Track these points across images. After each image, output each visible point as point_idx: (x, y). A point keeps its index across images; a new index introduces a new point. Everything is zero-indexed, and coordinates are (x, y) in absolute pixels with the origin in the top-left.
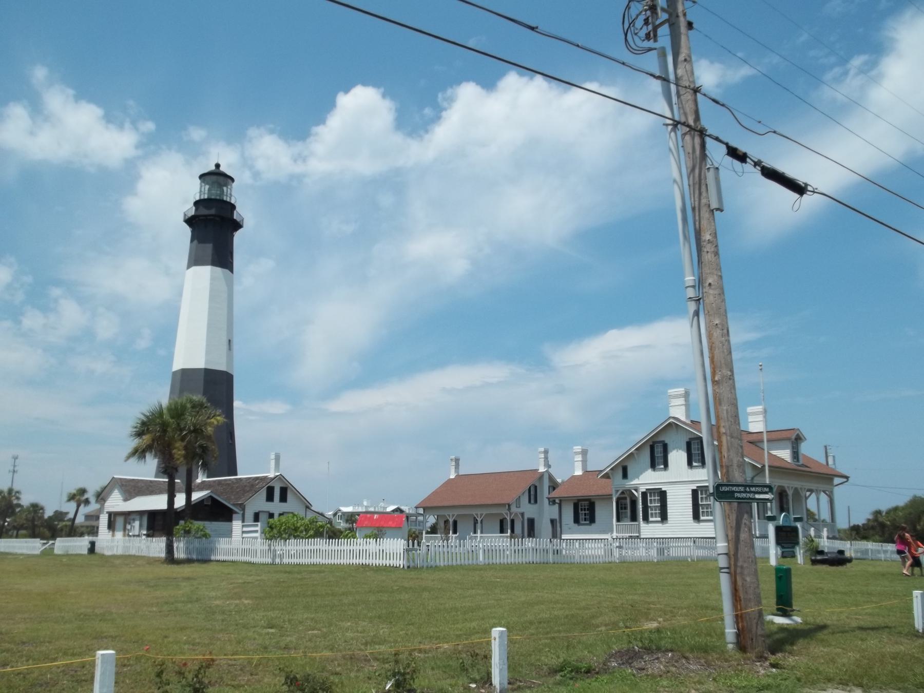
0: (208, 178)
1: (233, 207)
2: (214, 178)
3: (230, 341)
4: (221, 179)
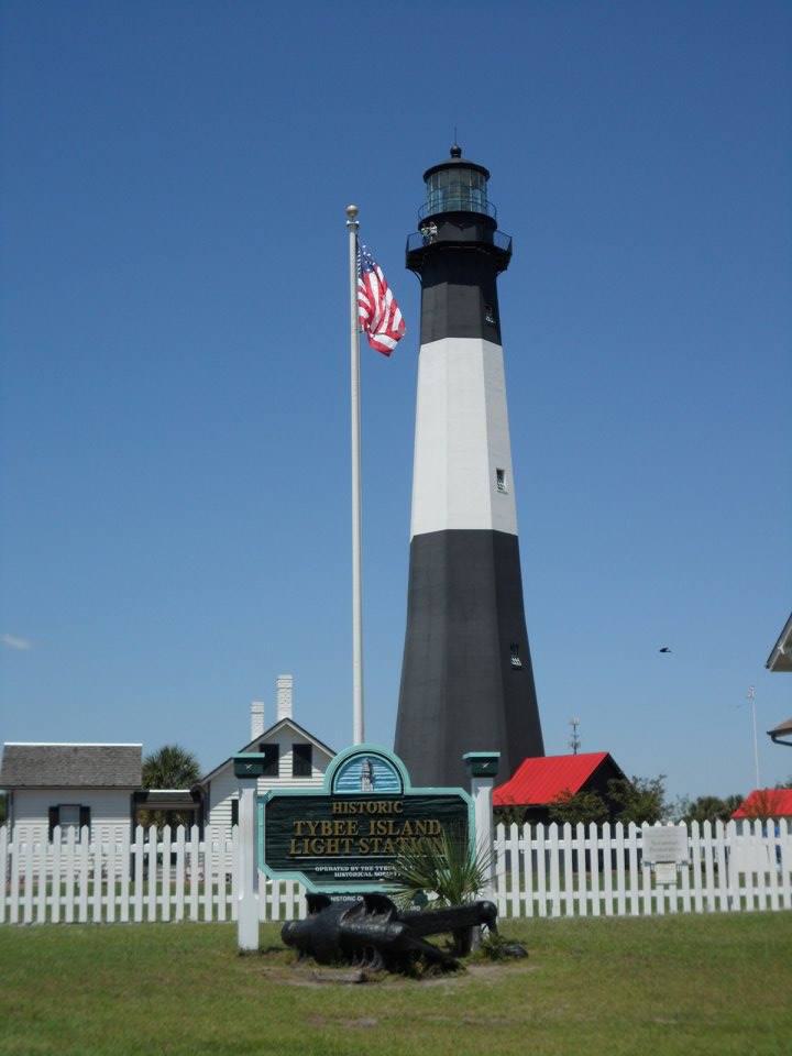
0: (442, 178)
2: (453, 174)
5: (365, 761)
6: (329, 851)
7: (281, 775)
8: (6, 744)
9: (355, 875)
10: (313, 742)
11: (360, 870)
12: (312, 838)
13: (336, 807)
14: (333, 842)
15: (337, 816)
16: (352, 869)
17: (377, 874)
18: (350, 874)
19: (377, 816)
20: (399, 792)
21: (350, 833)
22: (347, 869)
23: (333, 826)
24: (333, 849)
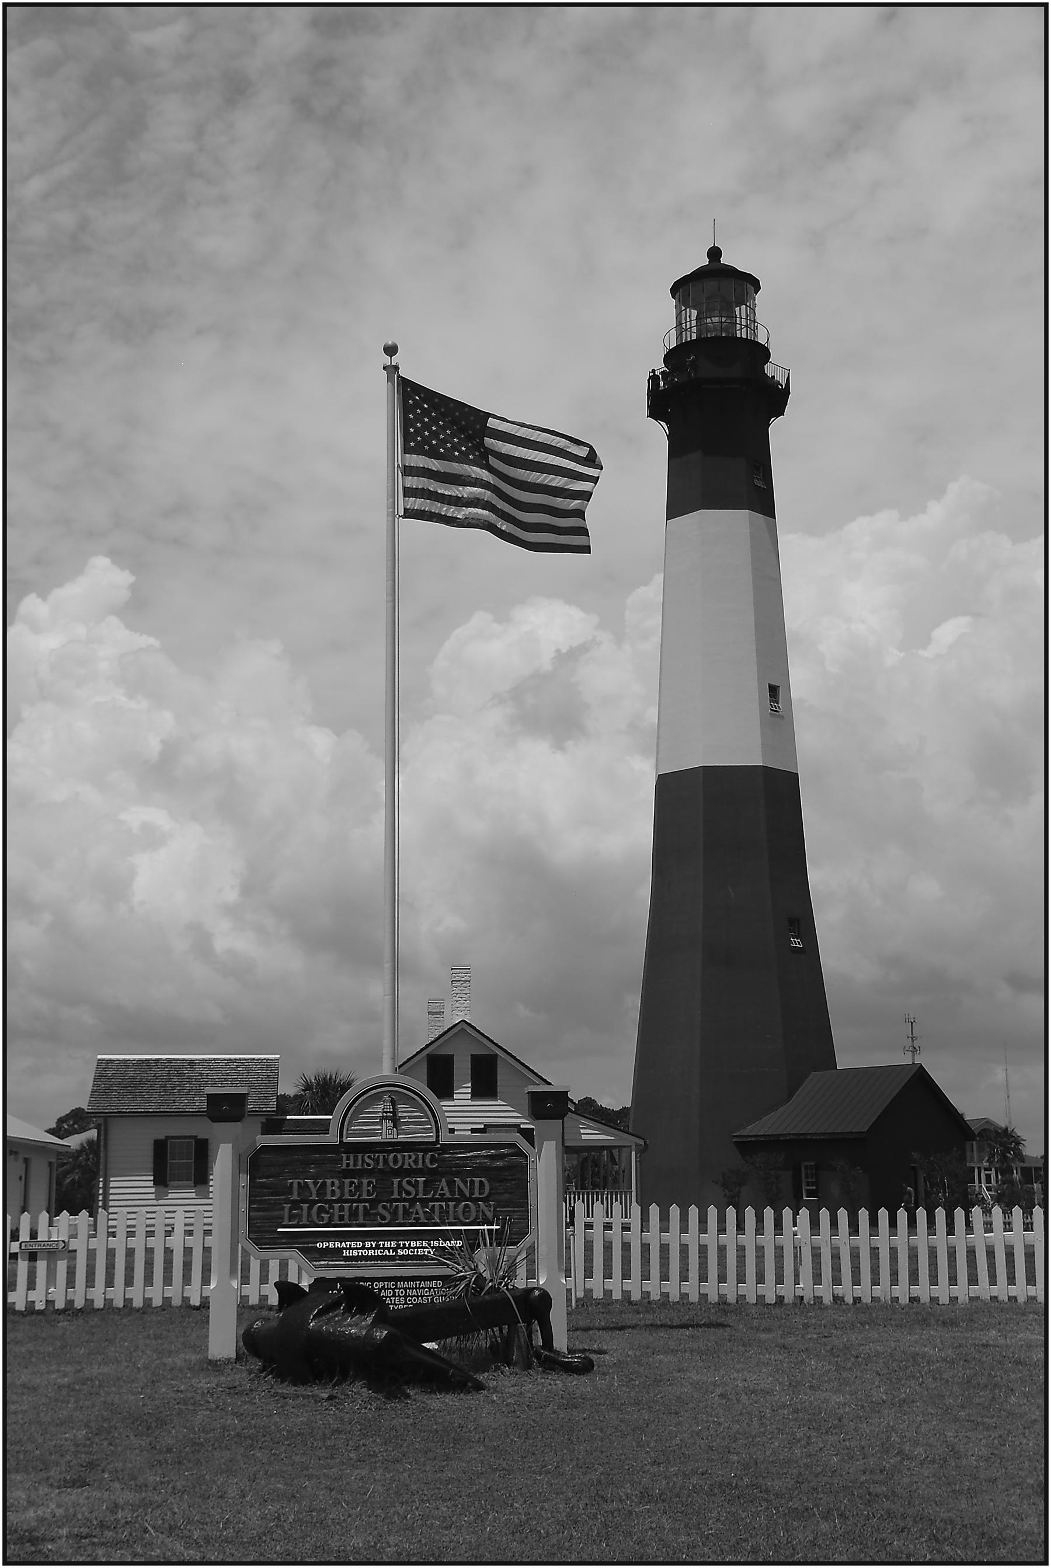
1: (763, 353)
2: (711, 284)
3: (774, 691)
6: (304, 1221)
8: (99, 1057)
9: (371, 1252)
10: (426, 1052)
12: (313, 1203)
13: (347, 1161)
14: (342, 1209)
15: (348, 1173)
16: (368, 1244)
17: (400, 1252)
19: (401, 1173)
21: (365, 1196)
22: (360, 1244)
23: (341, 1187)
24: (341, 1218)
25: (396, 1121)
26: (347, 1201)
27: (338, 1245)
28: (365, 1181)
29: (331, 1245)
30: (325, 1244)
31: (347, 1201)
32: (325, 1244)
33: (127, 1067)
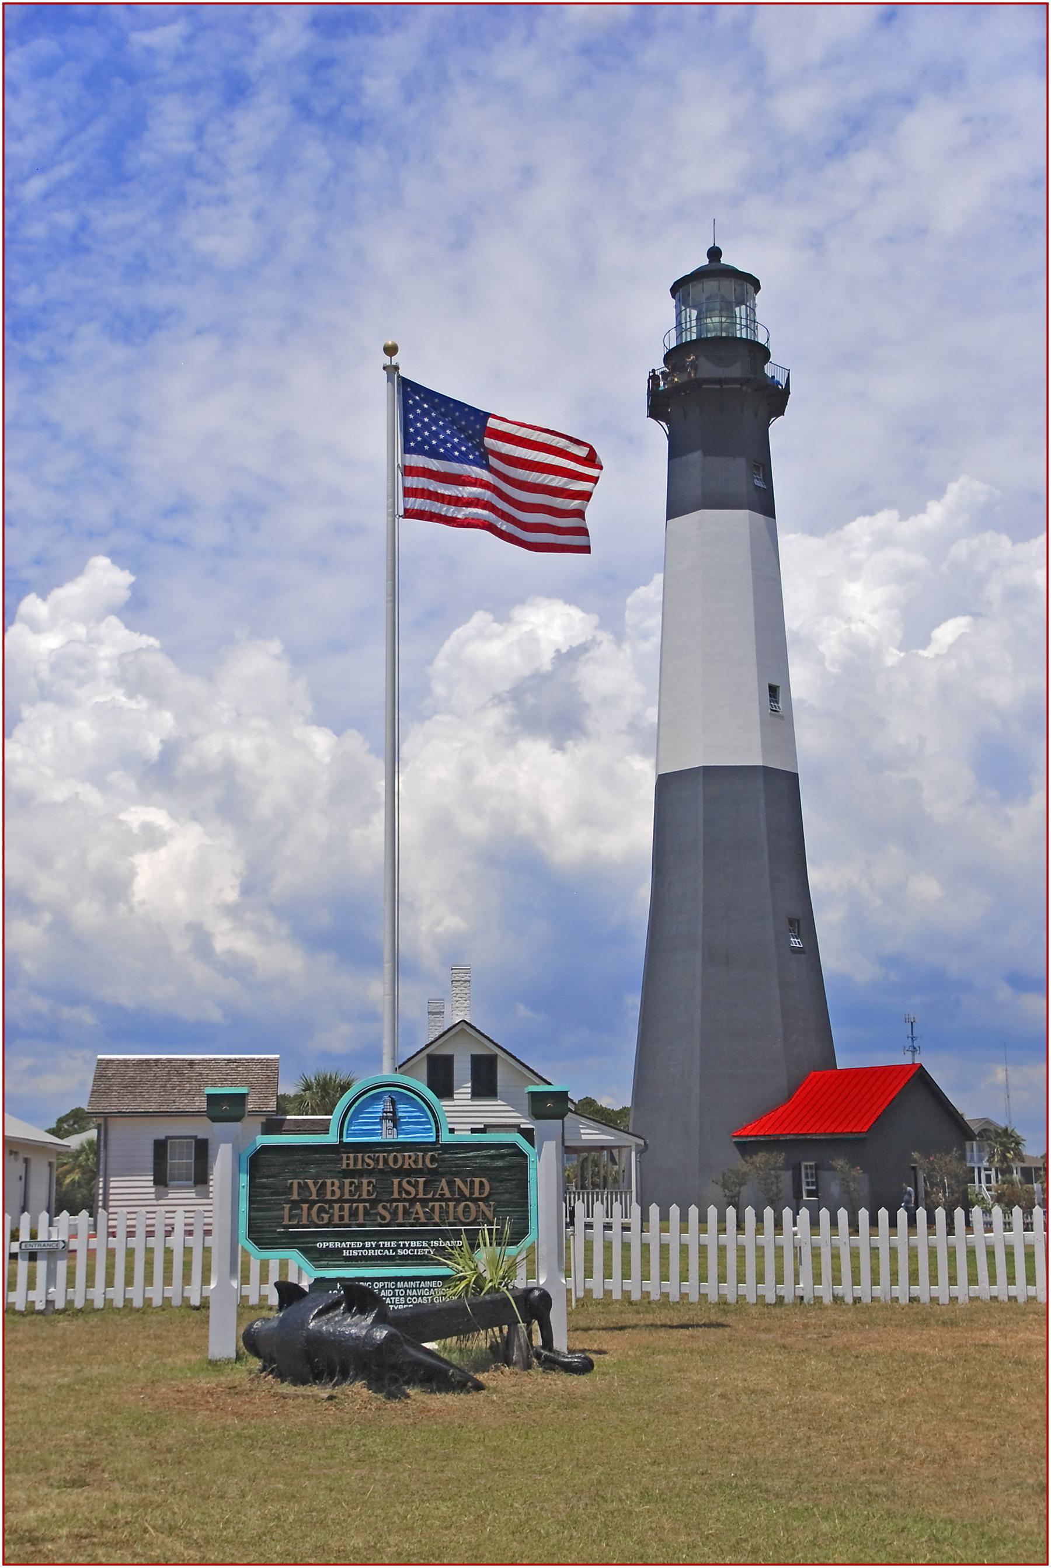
1: (763, 353)
2: (710, 285)
3: (773, 691)
4: (729, 287)
5: (386, 1097)
6: (346, 1221)
7: (455, 1096)
9: (371, 1253)
11: (378, 1247)
12: (312, 1203)
13: (347, 1161)
14: (341, 1209)
16: (368, 1244)
17: (400, 1252)
18: (365, 1252)
20: (433, 1140)
21: (365, 1196)
22: (360, 1244)
23: (341, 1187)
24: (341, 1218)
25: (396, 1121)
26: (347, 1201)
27: (338, 1245)
28: (365, 1181)
29: (331, 1245)
30: (325, 1245)
31: (347, 1201)
32: (325, 1245)
33: (127, 1066)
